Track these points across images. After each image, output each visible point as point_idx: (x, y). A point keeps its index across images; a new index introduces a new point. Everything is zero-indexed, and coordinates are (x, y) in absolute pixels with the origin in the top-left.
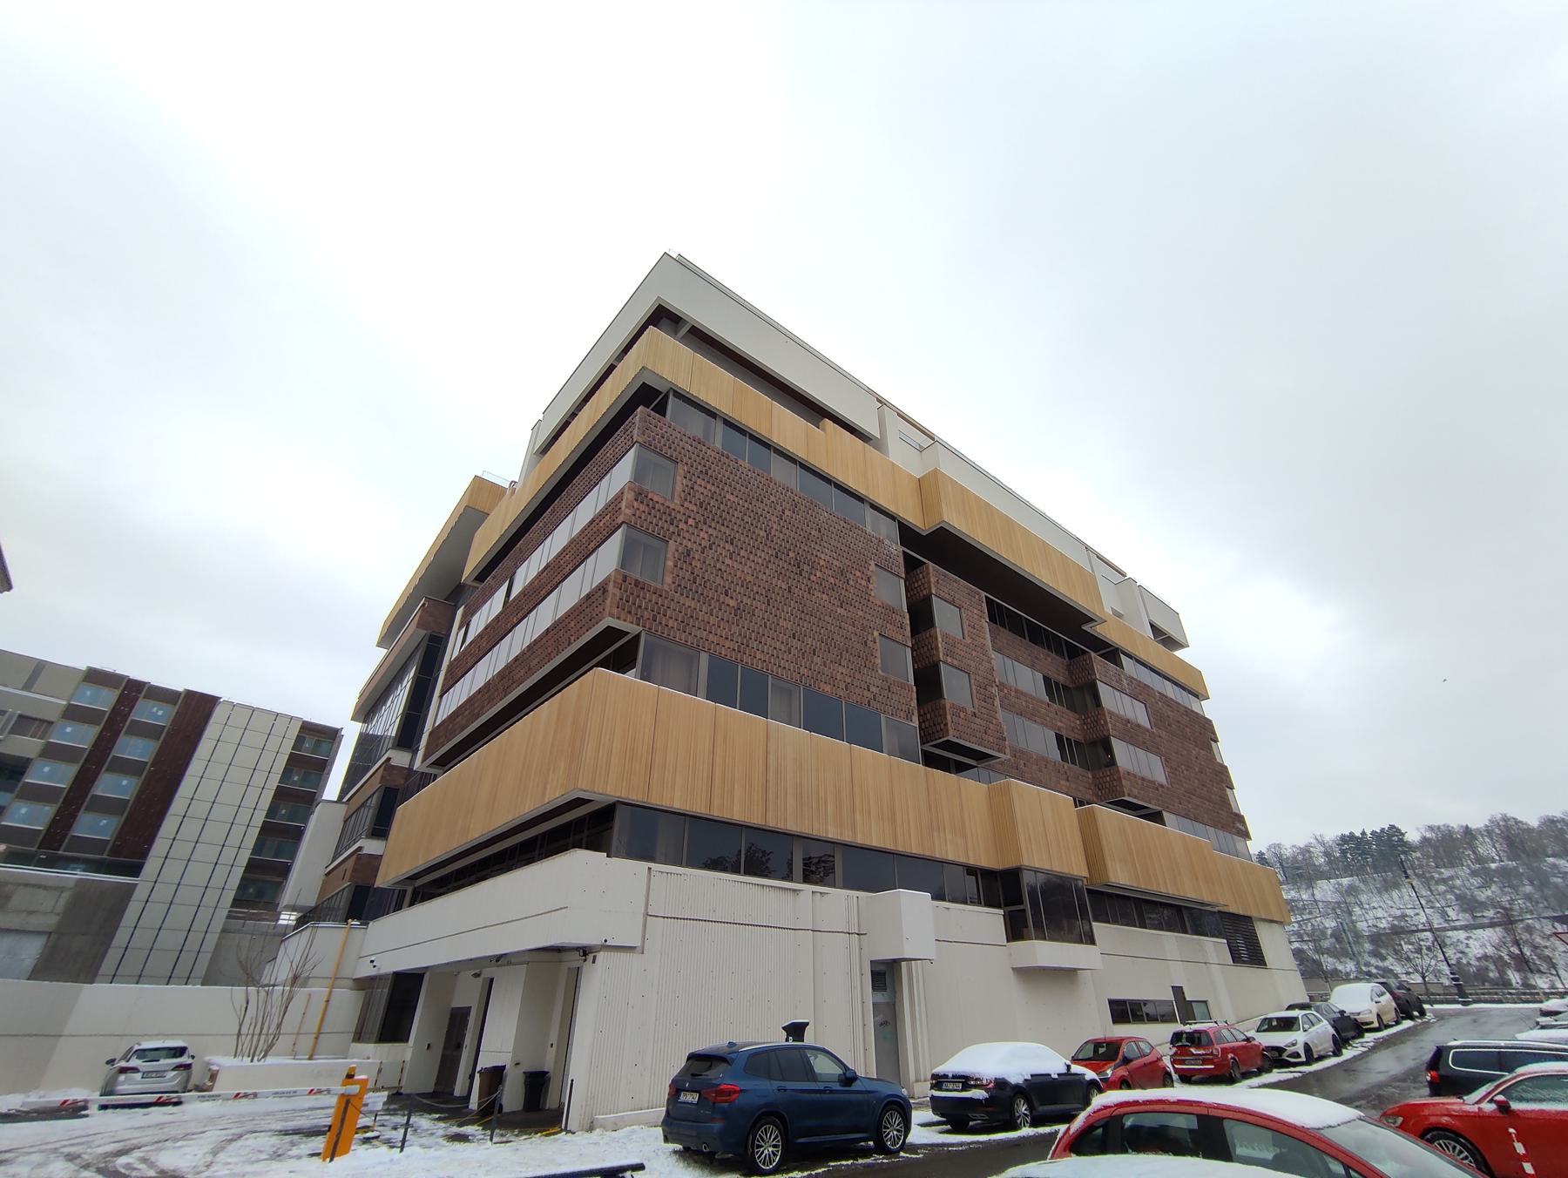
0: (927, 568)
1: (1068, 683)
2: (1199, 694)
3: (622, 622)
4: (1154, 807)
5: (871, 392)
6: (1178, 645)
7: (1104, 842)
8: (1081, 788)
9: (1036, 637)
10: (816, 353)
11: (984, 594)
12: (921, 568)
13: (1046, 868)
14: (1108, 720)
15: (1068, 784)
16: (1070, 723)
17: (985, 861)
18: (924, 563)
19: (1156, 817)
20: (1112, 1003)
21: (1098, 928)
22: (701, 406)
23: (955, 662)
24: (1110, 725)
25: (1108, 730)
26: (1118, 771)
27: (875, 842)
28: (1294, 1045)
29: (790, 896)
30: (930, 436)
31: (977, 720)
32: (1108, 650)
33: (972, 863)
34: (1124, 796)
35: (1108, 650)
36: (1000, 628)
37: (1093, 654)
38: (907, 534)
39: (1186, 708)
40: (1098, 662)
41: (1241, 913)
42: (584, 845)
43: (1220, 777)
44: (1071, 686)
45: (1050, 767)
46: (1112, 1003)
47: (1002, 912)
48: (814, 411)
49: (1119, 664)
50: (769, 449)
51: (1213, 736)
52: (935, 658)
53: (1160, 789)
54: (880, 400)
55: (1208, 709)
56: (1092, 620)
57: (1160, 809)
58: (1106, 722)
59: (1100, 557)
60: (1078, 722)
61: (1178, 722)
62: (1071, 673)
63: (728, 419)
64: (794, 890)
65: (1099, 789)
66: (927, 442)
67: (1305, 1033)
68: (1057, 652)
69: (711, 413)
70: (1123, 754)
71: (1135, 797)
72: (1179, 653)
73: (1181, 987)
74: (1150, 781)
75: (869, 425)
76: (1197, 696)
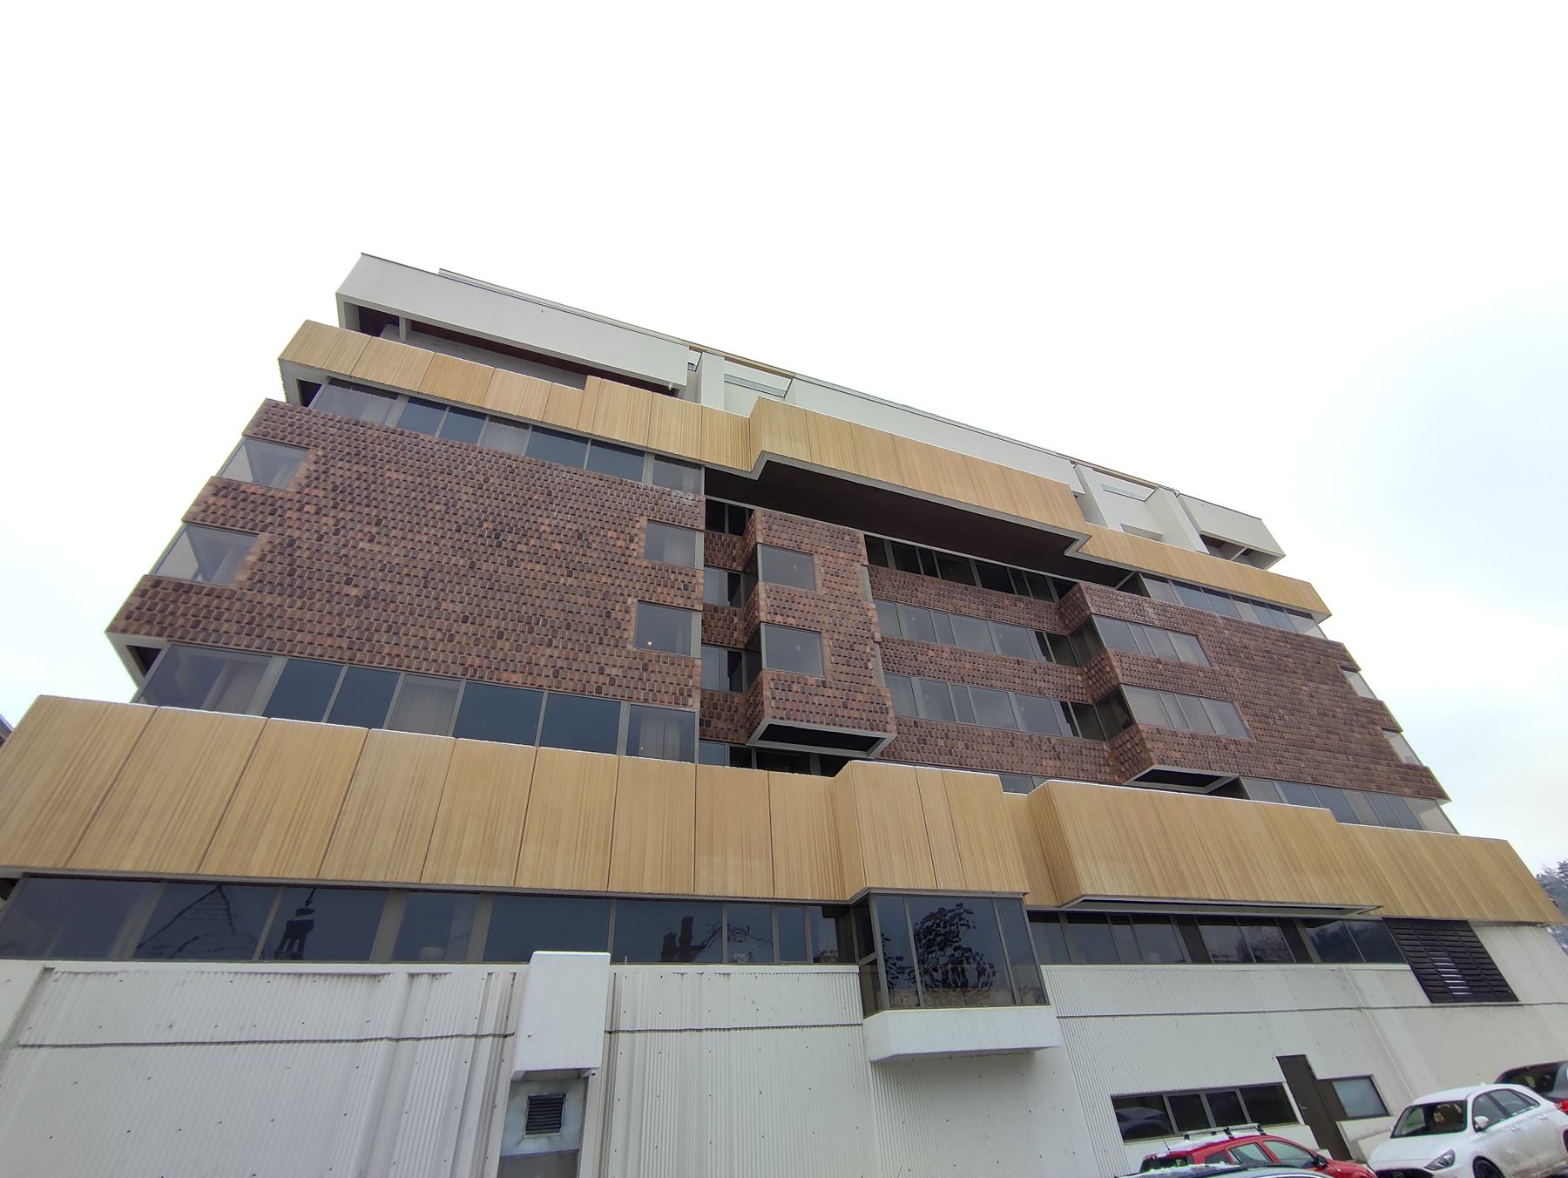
0: (1080, 589)
1: (1059, 631)
2: (1314, 612)
3: (857, 730)
4: (1231, 775)
5: (684, 342)
6: (1271, 558)
7: (1070, 835)
8: (1085, 767)
9: (996, 581)
10: (620, 324)
11: (861, 534)
12: (1070, 593)
13: (930, 887)
14: (1115, 664)
15: (1058, 763)
16: (1069, 680)
17: (832, 895)
18: (1076, 583)
19: (1233, 789)
20: (1119, 1102)
21: (1054, 976)
22: (498, 417)
23: (791, 621)
24: (1118, 671)
25: (1117, 678)
26: (1139, 731)
27: (560, 881)
28: (1447, 1164)
29: (361, 987)
30: (791, 376)
31: (827, 692)
32: (1128, 577)
33: (810, 898)
34: (1152, 764)
35: (1128, 577)
36: (926, 577)
37: (1083, 584)
38: (717, 480)
39: (1282, 632)
40: (1094, 596)
41: (1434, 915)
42: (725, 959)
43: (1376, 717)
44: (1065, 633)
45: (1020, 744)
46: (1119, 1102)
47: (855, 968)
48: (573, 371)
49: (1141, 591)
50: (1229, 598)
51: (1345, 663)
52: (1114, 683)
53: (1232, 747)
54: (1074, 462)
55: (1331, 630)
56: (1073, 540)
57: (1234, 775)
58: (1112, 667)
59: (1097, 469)
60: (1080, 678)
61: (1268, 652)
62: (1062, 616)
63: (598, 439)
64: (375, 976)
65: (1122, 764)
66: (782, 383)
67: (1480, 1134)
68: (1036, 595)
69: (392, 394)
70: (1145, 708)
71: (1176, 763)
72: (1276, 569)
73: (1304, 1056)
74: (1208, 738)
75: (674, 375)
76: (1308, 616)
